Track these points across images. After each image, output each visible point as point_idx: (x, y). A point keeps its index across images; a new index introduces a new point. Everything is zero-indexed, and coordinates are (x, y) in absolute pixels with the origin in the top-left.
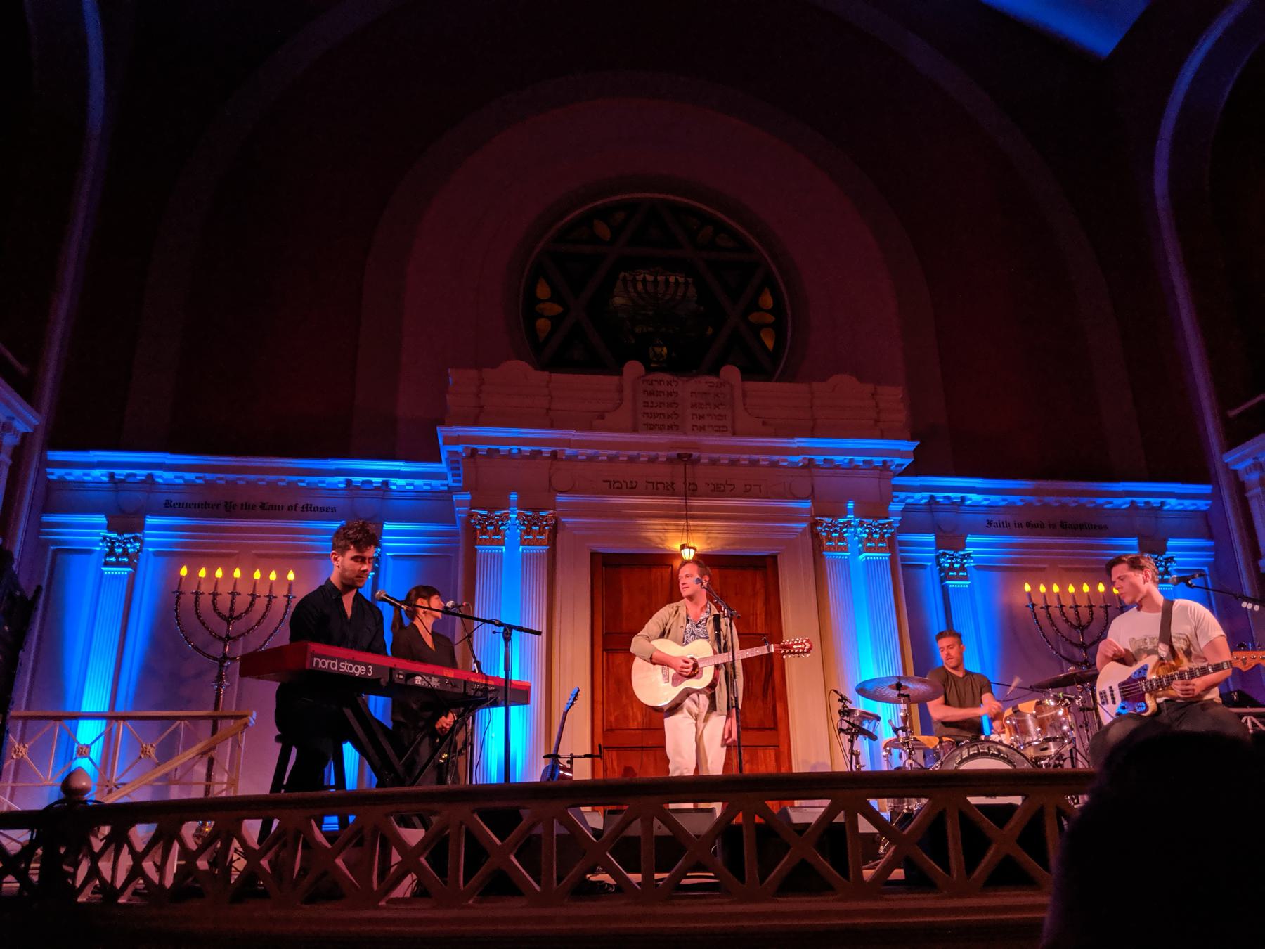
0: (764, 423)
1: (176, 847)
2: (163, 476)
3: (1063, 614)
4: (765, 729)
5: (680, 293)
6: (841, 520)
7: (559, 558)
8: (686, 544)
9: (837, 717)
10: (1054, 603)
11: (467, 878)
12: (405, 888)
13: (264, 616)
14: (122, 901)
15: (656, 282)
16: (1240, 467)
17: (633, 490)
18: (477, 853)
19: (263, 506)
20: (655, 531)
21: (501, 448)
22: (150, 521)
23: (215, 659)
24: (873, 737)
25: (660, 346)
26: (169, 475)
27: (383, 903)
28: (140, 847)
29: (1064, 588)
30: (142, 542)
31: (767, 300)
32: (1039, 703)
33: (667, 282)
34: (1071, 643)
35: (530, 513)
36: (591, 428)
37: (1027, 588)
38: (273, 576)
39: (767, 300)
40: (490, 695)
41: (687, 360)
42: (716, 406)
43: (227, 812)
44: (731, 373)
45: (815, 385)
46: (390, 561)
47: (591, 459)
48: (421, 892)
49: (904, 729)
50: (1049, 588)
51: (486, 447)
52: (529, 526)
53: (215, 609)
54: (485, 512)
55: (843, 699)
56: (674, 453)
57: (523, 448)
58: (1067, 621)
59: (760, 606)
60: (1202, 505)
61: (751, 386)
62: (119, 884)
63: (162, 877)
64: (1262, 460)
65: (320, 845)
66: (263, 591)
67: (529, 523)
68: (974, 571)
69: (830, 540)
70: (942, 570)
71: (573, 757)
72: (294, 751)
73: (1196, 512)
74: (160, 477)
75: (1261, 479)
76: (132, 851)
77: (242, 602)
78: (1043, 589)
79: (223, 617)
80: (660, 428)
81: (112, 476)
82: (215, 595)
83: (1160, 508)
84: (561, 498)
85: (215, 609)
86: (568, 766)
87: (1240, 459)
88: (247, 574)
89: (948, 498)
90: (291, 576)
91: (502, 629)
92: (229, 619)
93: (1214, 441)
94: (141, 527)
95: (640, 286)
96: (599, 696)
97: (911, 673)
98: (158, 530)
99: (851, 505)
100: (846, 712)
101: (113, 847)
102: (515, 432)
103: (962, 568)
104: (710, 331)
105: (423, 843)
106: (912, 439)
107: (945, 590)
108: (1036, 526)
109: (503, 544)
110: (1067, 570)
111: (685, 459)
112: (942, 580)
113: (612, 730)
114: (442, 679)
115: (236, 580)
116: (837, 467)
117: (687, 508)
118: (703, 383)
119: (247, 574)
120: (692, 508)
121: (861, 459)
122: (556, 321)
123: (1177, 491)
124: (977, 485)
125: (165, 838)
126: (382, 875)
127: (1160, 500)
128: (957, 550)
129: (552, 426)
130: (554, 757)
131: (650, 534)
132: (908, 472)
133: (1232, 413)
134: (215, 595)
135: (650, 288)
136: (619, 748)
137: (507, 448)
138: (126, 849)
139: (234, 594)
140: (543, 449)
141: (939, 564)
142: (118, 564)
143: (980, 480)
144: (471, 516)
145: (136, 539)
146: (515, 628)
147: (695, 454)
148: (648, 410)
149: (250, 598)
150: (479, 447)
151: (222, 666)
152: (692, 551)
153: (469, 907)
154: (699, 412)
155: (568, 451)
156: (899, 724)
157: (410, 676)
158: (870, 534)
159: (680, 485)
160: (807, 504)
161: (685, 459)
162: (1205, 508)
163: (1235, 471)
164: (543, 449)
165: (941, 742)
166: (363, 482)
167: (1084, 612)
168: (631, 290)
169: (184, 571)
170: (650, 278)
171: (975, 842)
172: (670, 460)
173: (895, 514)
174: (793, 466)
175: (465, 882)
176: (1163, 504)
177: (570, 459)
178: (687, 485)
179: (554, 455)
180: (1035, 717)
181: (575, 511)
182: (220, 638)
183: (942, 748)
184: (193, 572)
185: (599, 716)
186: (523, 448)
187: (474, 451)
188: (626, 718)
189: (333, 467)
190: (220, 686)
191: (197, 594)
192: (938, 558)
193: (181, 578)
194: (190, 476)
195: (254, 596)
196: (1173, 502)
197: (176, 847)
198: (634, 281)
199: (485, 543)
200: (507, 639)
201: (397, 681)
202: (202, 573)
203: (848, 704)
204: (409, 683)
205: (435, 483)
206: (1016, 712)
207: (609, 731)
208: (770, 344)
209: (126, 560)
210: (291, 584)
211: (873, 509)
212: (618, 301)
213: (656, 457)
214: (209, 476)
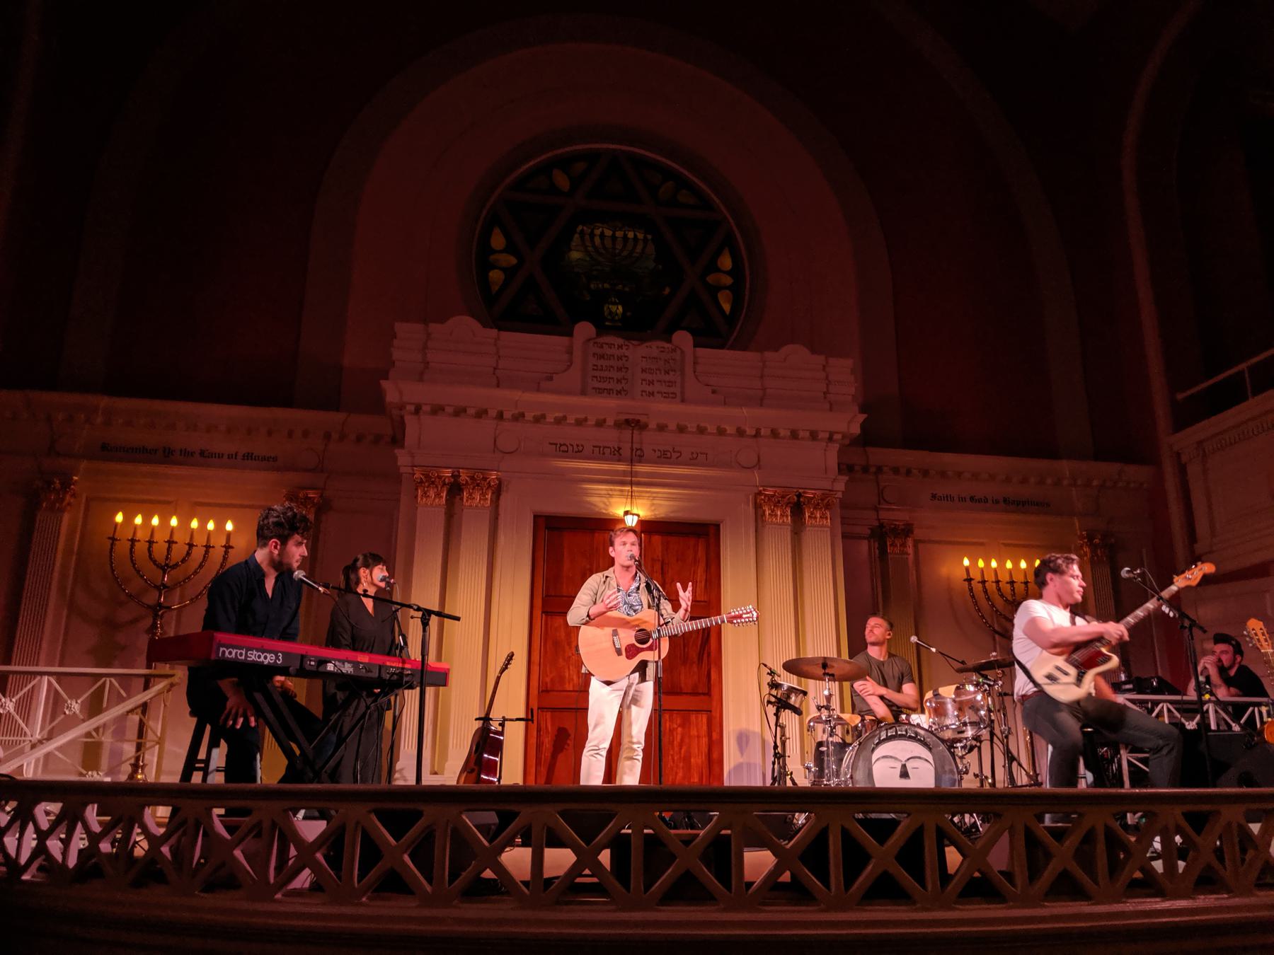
0: (714, 392)
3: (999, 590)
5: (639, 248)
8: (631, 510)
9: (766, 689)
11: (361, 876)
12: (304, 879)
13: (201, 566)
14: (26, 877)
15: (614, 238)
18: (372, 852)
19: (202, 453)
20: (600, 496)
25: (614, 303)
27: (279, 896)
28: (44, 824)
31: (726, 262)
32: (958, 688)
33: (625, 238)
37: (966, 562)
38: (211, 526)
39: (726, 262)
40: (405, 679)
41: (642, 323)
42: (667, 372)
43: (125, 800)
44: (683, 338)
45: (768, 354)
48: (316, 887)
49: (827, 708)
50: (988, 563)
55: (772, 673)
58: (1002, 596)
61: (702, 352)
62: (23, 860)
63: (65, 853)
65: (219, 836)
66: (200, 541)
71: (505, 720)
72: (208, 728)
76: (37, 829)
77: (179, 551)
78: (981, 564)
86: (500, 729)
90: (229, 526)
91: (420, 614)
92: (164, 568)
95: (597, 240)
100: (774, 685)
101: (18, 823)
104: (667, 291)
105: (322, 839)
108: (980, 501)
113: (547, 691)
115: (173, 528)
117: (632, 474)
118: (653, 348)
122: (510, 272)
125: (69, 818)
126: (279, 869)
130: (486, 719)
131: (595, 500)
133: (1180, 396)
134: (151, 542)
135: (608, 243)
136: (553, 710)
138: (31, 827)
139: (171, 542)
146: (434, 612)
147: (643, 419)
148: (597, 373)
152: (636, 518)
153: (361, 904)
154: (649, 377)
157: (322, 662)
159: (626, 452)
165: (863, 720)
168: (588, 244)
169: (119, 518)
170: (608, 233)
171: (855, 857)
172: (618, 425)
175: (359, 882)
178: (632, 452)
180: (954, 701)
183: (863, 725)
184: (129, 518)
185: (535, 677)
188: (562, 678)
191: (133, 541)
193: (116, 524)
195: (191, 545)
198: (592, 235)
200: (425, 624)
201: (308, 668)
202: (138, 520)
204: (321, 669)
206: (936, 695)
207: (544, 691)
208: (727, 307)
210: (229, 535)
212: (575, 255)
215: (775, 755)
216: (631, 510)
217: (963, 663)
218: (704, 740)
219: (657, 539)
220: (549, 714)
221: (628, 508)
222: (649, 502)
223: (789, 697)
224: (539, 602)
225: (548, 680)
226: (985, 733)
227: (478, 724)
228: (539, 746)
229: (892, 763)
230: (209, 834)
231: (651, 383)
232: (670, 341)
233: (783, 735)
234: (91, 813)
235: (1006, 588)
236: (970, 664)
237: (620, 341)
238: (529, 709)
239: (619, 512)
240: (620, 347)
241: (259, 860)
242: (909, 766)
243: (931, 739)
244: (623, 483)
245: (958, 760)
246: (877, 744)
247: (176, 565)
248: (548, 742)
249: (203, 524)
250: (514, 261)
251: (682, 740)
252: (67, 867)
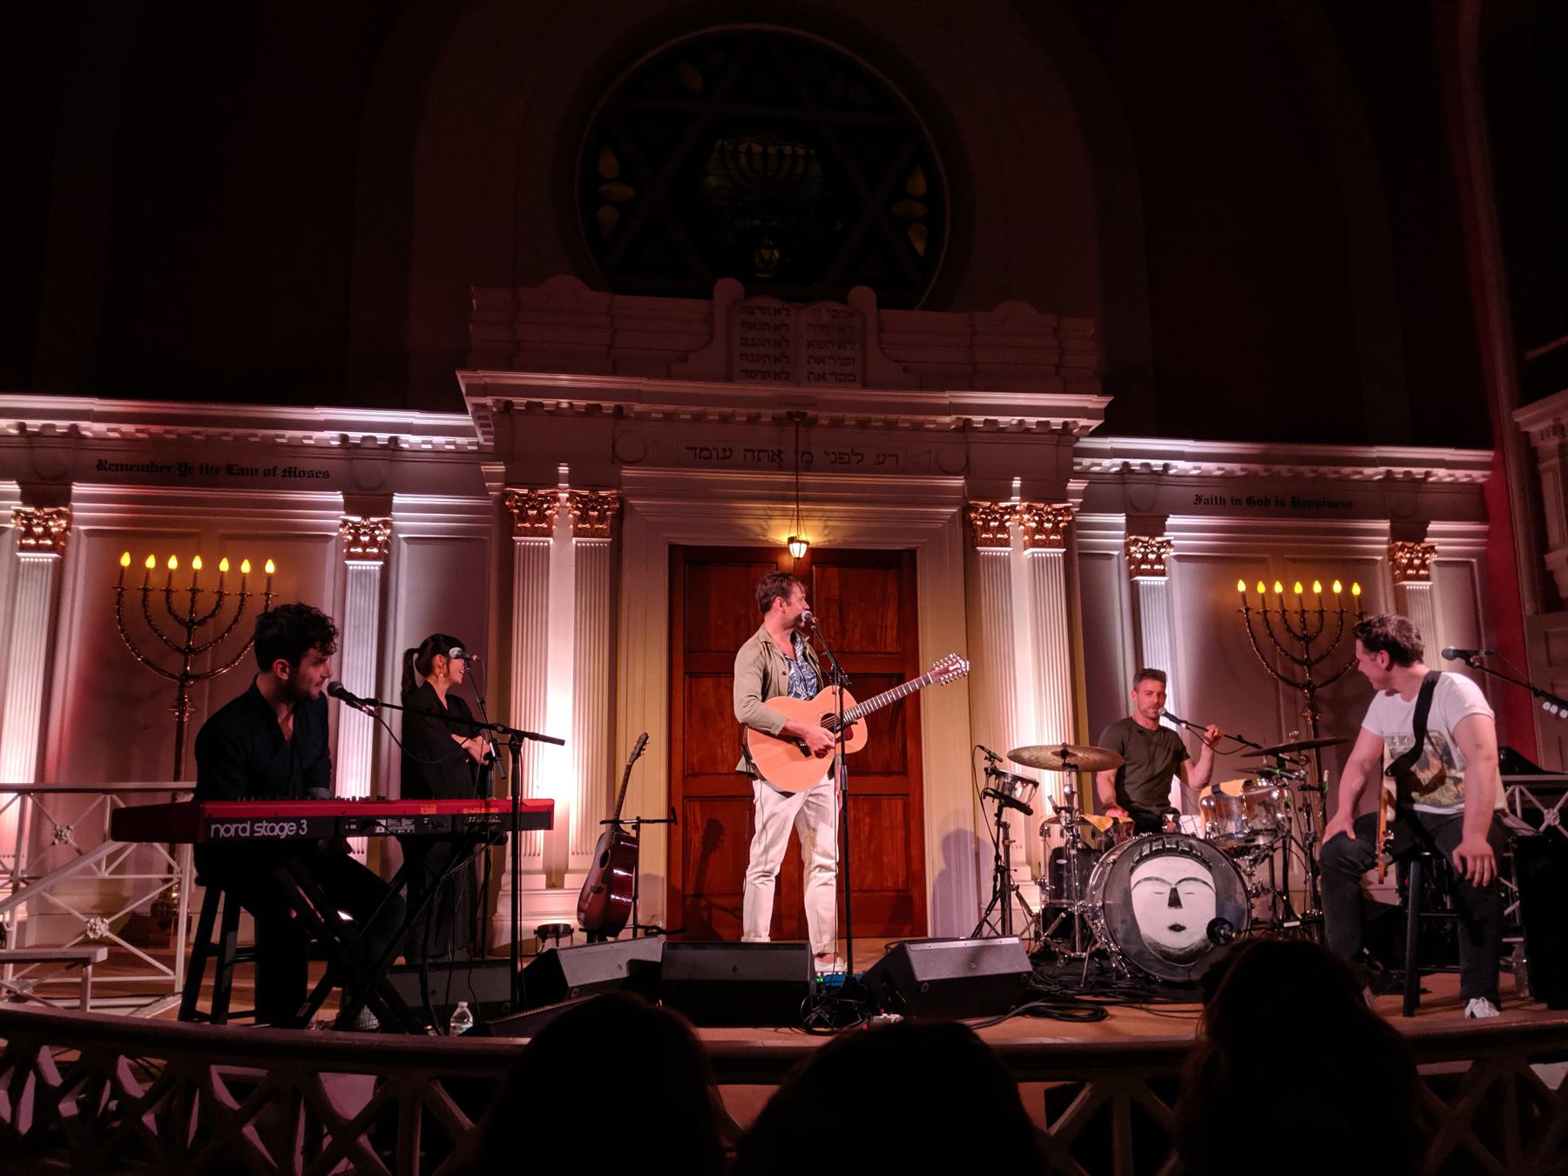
0: (906, 370)
1: (31, 1080)
2: (90, 428)
4: (890, 774)
6: (1003, 505)
7: (626, 550)
9: (982, 776)
10: (1275, 606)
13: (236, 620)
16: (1533, 429)
17: (725, 460)
19: (229, 469)
20: (757, 517)
21: (546, 401)
22: (78, 489)
23: (172, 676)
24: (1027, 810)
26: (100, 427)
29: (1288, 587)
30: (69, 518)
31: (919, 184)
34: (1293, 658)
35: (585, 493)
36: (669, 375)
37: (1242, 586)
39: (919, 184)
44: (863, 296)
46: (404, 545)
47: (668, 417)
49: (1069, 810)
50: (1270, 587)
51: (524, 400)
52: (585, 512)
53: (170, 609)
54: (525, 491)
55: (991, 757)
56: (782, 411)
57: (576, 402)
58: (1289, 630)
59: (891, 617)
60: (1478, 475)
61: (888, 314)
64: (1564, 422)
65: (220, 1105)
66: (232, 588)
67: (585, 506)
68: (1175, 562)
69: (986, 529)
70: (1132, 561)
71: (640, 821)
73: (1472, 484)
74: (87, 429)
75: (1561, 446)
77: (206, 602)
79: (181, 621)
80: (763, 376)
81: (22, 427)
82: (168, 591)
83: (1424, 480)
84: (628, 472)
85: (170, 609)
87: (1535, 420)
88: (211, 563)
89: (1148, 465)
90: (270, 567)
93: (1503, 384)
94: (66, 498)
95: (743, 159)
96: (678, 732)
97: (1085, 741)
98: (90, 502)
99: (1017, 483)
100: (993, 772)
102: (564, 380)
103: (1159, 560)
106: (1103, 393)
107: (1134, 589)
109: (549, 535)
110: (1293, 561)
111: (796, 419)
112: (1131, 574)
114: (418, 819)
115: (196, 572)
116: (1003, 430)
117: (798, 486)
119: (211, 563)
120: (804, 487)
121: (1034, 420)
123: (1448, 458)
124: (1187, 449)
127: (1423, 470)
128: (1153, 536)
129: (614, 373)
130: (615, 823)
132: (1099, 433)
136: (703, 799)
137: (553, 401)
140: (604, 404)
141: (1128, 553)
142: (38, 548)
143: (1191, 443)
144: (506, 496)
145: (60, 515)
147: (811, 413)
149: (216, 597)
150: (515, 400)
151: (183, 686)
152: (804, 547)
155: (638, 407)
156: (1062, 803)
158: (1040, 523)
160: (958, 482)
161: (796, 419)
162: (1481, 480)
163: (1527, 434)
164: (604, 404)
166: (364, 439)
167: (1313, 619)
170: (757, 149)
172: (777, 421)
173: (1076, 494)
174: (943, 429)
176: (1428, 474)
177: (641, 416)
178: (798, 457)
179: (619, 410)
181: (647, 489)
182: (179, 649)
184: (138, 560)
186: (576, 402)
187: (509, 405)
189: (322, 418)
190: (182, 713)
192: (1127, 545)
194: (127, 428)
195: (220, 594)
196: (1441, 473)
197: (31, 1080)
199: (525, 532)
202: (151, 562)
203: (997, 763)
205: (460, 440)
207: (691, 774)
208: (920, 247)
209: (49, 542)
211: (1046, 489)
213: (759, 416)
214: (155, 429)
215: (998, 869)
216: (797, 536)
217: (1255, 746)
218: (900, 833)
219: (832, 572)
220: (697, 805)
221: (793, 534)
222: (821, 524)
223: (1013, 788)
224: (679, 648)
225: (695, 760)
226: (1279, 844)
227: (604, 828)
228: (686, 844)
229: (1158, 887)
230: (209, 1098)
231: (820, 361)
232: (844, 301)
233: (1006, 836)
234: (47, 1057)
235: (1295, 620)
236: (1265, 748)
237: (777, 304)
238: (671, 810)
239: (783, 539)
240: (777, 312)
241: (279, 1139)
242: (1181, 890)
243: (1208, 851)
244: (785, 499)
245: (1246, 878)
246: (1138, 862)
247: (203, 622)
248: (696, 839)
249: (235, 565)
250: (630, 192)
251: (871, 833)
252: (18, 1132)
